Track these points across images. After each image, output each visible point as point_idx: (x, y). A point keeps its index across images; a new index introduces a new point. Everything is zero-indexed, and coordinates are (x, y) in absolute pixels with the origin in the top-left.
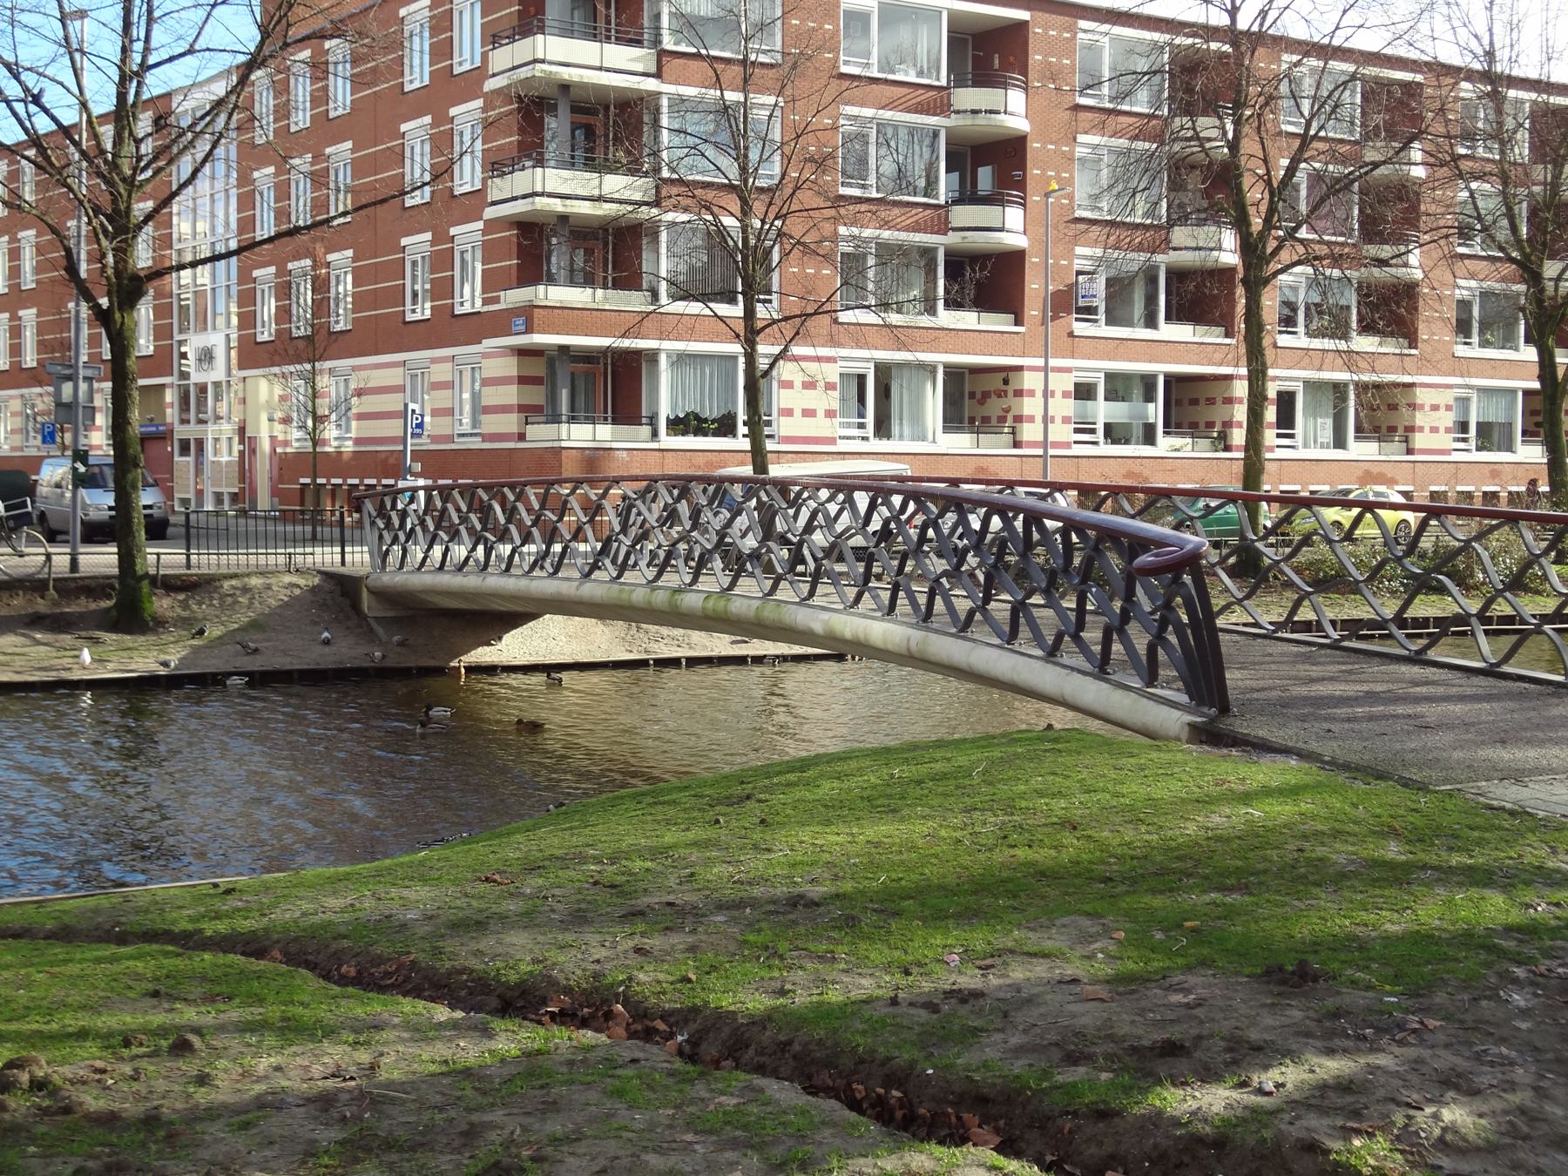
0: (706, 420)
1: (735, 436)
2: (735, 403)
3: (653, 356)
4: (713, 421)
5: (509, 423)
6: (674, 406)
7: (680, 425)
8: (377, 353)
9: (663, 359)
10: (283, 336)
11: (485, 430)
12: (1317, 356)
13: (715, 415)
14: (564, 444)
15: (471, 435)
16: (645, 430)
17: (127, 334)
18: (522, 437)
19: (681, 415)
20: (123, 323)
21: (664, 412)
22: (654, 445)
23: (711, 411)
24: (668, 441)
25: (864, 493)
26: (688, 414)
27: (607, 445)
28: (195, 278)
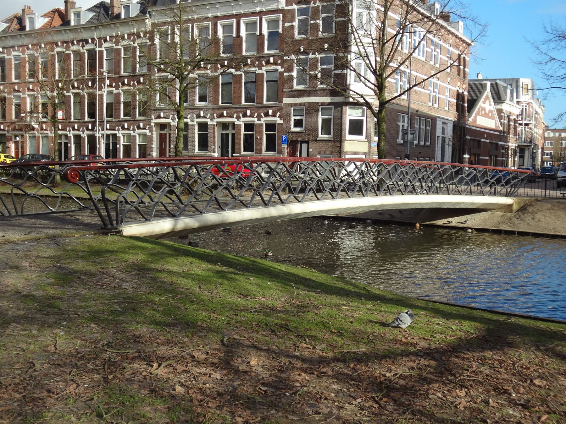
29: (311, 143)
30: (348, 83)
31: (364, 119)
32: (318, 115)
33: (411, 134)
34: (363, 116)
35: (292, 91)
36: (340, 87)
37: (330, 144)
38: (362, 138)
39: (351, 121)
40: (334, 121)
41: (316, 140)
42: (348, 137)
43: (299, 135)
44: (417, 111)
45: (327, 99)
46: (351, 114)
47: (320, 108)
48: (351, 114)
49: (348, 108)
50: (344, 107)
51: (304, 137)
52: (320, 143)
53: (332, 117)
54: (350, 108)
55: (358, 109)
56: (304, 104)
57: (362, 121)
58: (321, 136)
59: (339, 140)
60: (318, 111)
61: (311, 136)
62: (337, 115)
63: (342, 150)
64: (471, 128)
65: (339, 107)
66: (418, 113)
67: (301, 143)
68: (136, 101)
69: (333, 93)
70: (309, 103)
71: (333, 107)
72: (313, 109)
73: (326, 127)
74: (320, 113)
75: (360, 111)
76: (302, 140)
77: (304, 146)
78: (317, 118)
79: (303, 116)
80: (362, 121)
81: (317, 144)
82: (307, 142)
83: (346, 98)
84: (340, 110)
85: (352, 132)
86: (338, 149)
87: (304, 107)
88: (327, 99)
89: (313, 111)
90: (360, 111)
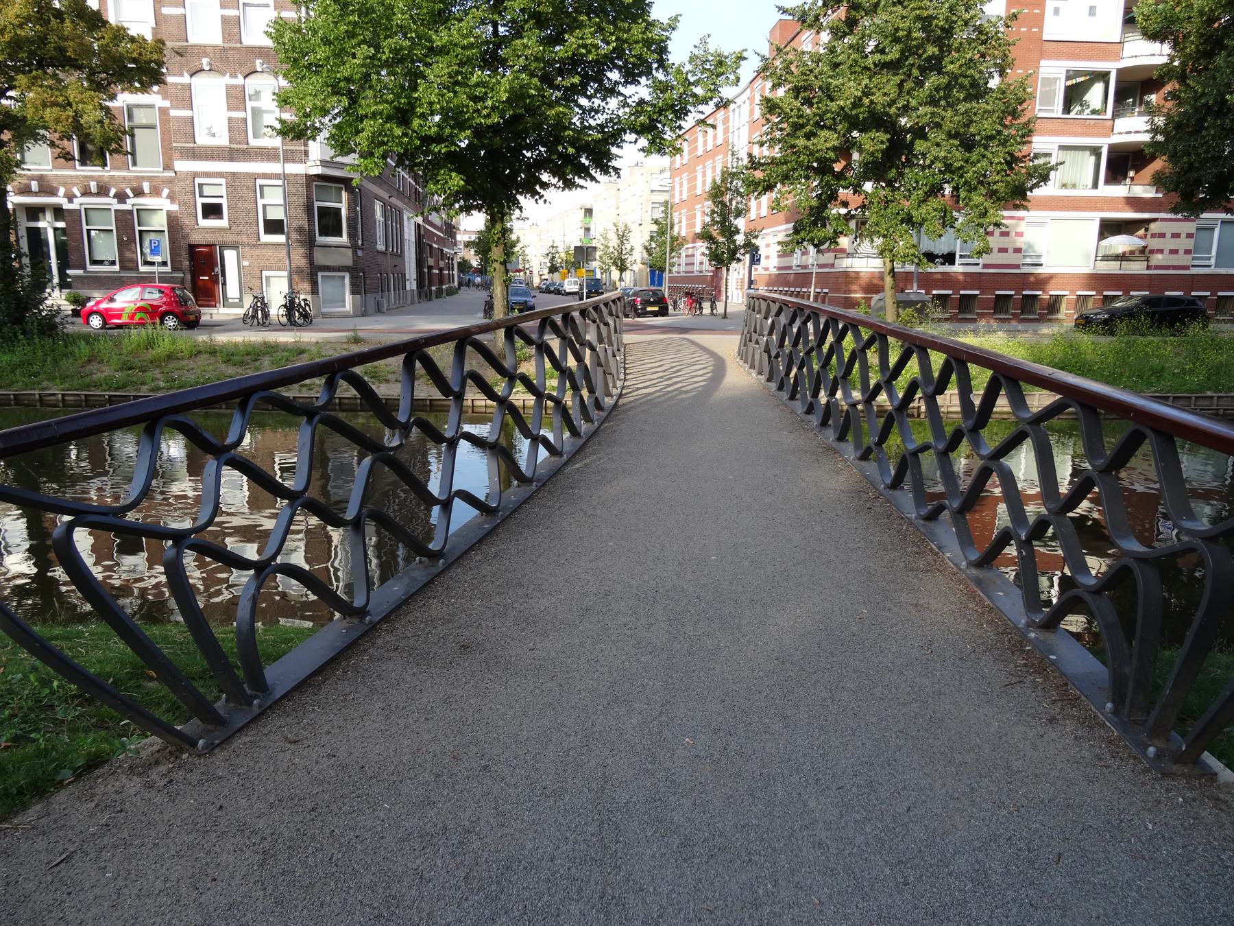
18: (833, 265)
61: (244, 237)
70: (234, 174)
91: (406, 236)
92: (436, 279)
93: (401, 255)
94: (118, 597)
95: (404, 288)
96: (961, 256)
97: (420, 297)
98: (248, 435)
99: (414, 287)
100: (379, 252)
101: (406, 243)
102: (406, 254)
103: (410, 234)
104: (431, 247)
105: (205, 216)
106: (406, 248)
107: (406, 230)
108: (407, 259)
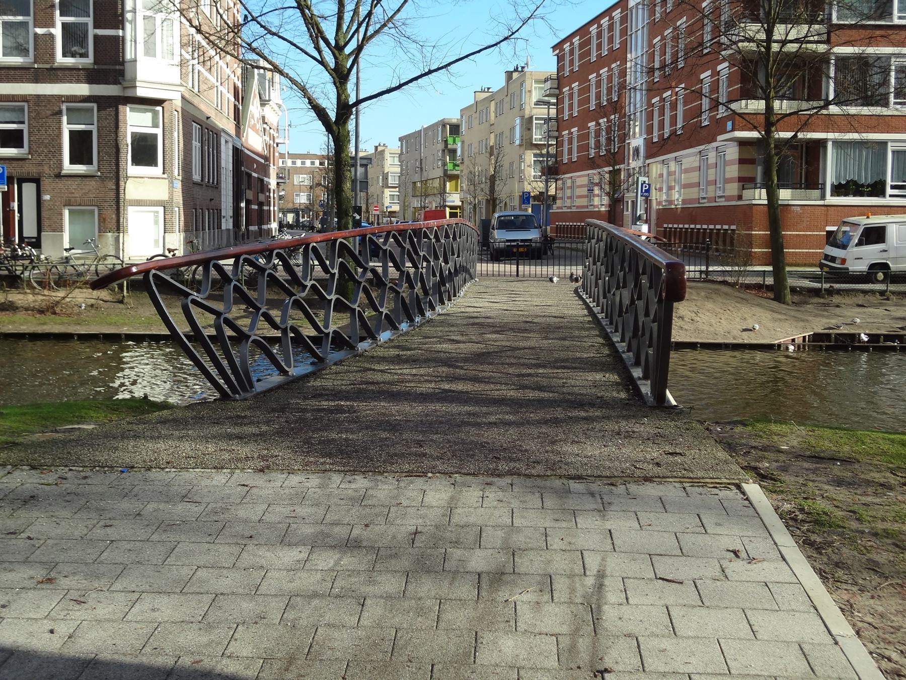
0: (862, 186)
1: (884, 196)
2: (884, 173)
3: (822, 143)
4: (868, 186)
5: (733, 189)
6: (838, 177)
7: (839, 190)
8: (61, 154)
9: (830, 145)
10: (673, 133)
11: (577, 204)
12: (811, 169)
13: (869, 181)
14: (754, 202)
15: (164, 247)
16: (817, 193)
17: (342, 138)
18: (740, 197)
19: (843, 182)
20: (339, 132)
21: (830, 179)
22: (821, 203)
23: (866, 179)
24: (831, 200)
25: (681, 309)
26: (848, 182)
27: (786, 202)
28: (747, 105)
29: (46, 183)
30: (128, 56)
31: (159, 131)
32: (60, 122)
33: (361, 165)
34: (155, 125)
35: (52, 69)
36: (111, 65)
37: (93, 183)
38: (157, 171)
39: (135, 136)
40: (99, 137)
41: (59, 176)
42: (133, 170)
43: (15, 164)
44: (208, 118)
45: (82, 89)
46: (135, 122)
47: (64, 107)
48: (135, 122)
49: (128, 109)
50: (121, 107)
51: (30, 169)
52: (69, 182)
53: (94, 128)
54: (132, 110)
55: (146, 111)
56: (24, 98)
57: (155, 136)
58: (68, 167)
59: (116, 177)
60: (60, 113)
61: (46, 168)
62: (105, 123)
63: (122, 196)
64: (246, 151)
65: (110, 106)
66: (208, 122)
67: (21, 181)
68: (836, 78)
69: (91, 76)
70: (38, 96)
71: (95, 106)
72: (46, 110)
73: (80, 152)
74: (65, 119)
75: (149, 115)
76: (25, 176)
77: (29, 190)
78: (59, 129)
79: (23, 123)
80: (155, 136)
81: (60, 184)
82: (37, 181)
83: (125, 88)
84: (113, 113)
85: (137, 161)
86: (112, 194)
87: (25, 104)
88: (82, 89)
89: (49, 112)
90: (149, 115)
91: (223, 164)
92: (255, 217)
93: (217, 187)
94: (617, 384)
95: (219, 227)
96: (893, 187)
97: (236, 238)
98: (448, 184)
99: (231, 226)
100: (195, 184)
101: (223, 172)
102: (223, 185)
103: (227, 161)
104: (249, 176)
105: (20, 132)
106: (223, 178)
107: (223, 156)
108: (223, 192)
